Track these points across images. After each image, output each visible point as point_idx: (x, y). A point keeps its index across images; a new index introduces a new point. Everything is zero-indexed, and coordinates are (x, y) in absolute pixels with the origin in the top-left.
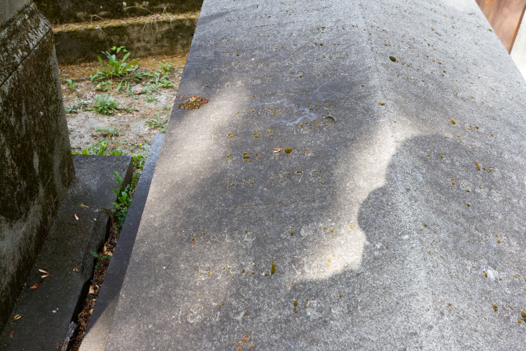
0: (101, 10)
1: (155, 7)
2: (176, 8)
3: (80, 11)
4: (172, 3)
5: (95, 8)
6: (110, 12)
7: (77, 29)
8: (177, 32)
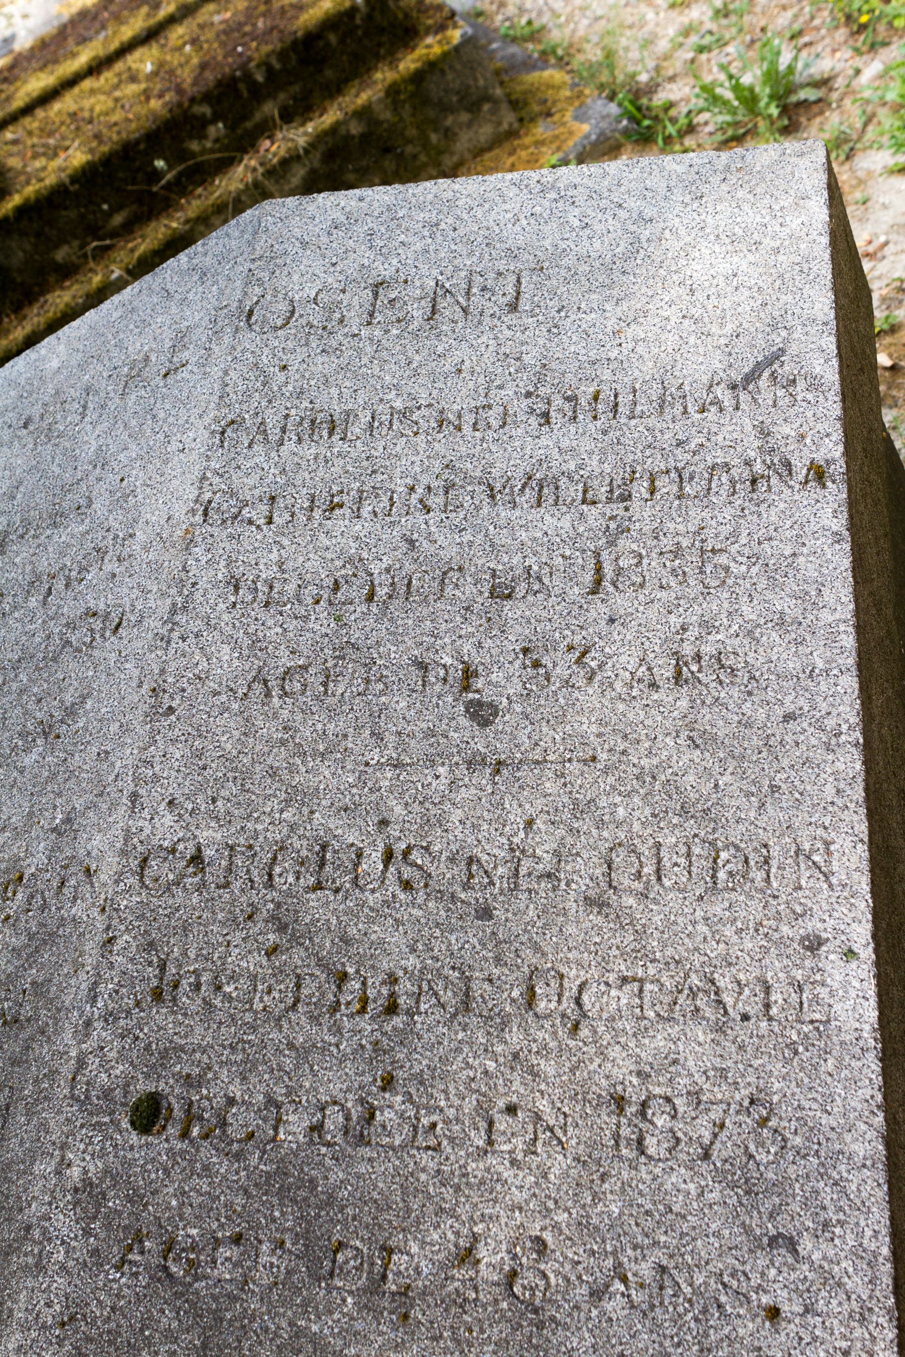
0: (110, 214)
1: (249, 125)
2: (311, 91)
3: (57, 247)
4: (291, 84)
5: (91, 217)
6: (134, 207)
7: (67, 305)
8: (335, 167)
